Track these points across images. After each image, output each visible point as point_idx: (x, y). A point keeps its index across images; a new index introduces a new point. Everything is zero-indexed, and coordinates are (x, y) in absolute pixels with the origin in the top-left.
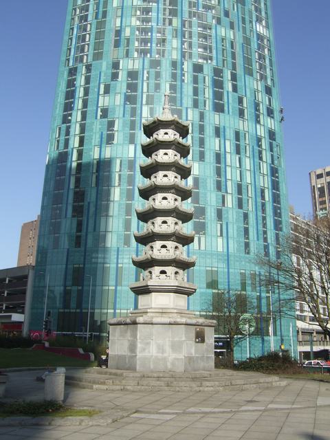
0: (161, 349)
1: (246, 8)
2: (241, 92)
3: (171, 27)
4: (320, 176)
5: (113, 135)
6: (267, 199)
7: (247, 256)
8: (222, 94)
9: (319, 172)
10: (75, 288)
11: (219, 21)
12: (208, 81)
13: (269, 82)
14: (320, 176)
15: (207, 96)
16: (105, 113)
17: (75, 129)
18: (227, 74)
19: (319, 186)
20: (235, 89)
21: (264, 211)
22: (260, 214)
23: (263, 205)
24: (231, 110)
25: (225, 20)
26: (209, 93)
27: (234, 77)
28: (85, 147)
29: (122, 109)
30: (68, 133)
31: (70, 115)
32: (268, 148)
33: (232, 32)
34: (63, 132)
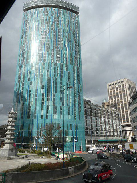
0: (5, 153)
1: (72, 43)
2: (69, 70)
3: (43, 84)
4: (110, 85)
5: (30, 116)
6: (76, 102)
7: (124, 81)
8: (63, 72)
9: (110, 84)
10: (21, 131)
11: (62, 49)
12: (59, 68)
13: (79, 66)
14: (110, 85)
15: (58, 73)
16: (29, 80)
17: (21, 84)
18: (64, 66)
19: (110, 89)
20: (67, 70)
21: (75, 106)
22: (74, 107)
23: (75, 104)
24: (65, 77)
25: (64, 48)
26: (59, 72)
27: (67, 66)
28: (24, 90)
29: (34, 78)
30: (19, 86)
31: (20, 80)
32: (77, 87)
33: (42, 113)
34: (18, 85)
